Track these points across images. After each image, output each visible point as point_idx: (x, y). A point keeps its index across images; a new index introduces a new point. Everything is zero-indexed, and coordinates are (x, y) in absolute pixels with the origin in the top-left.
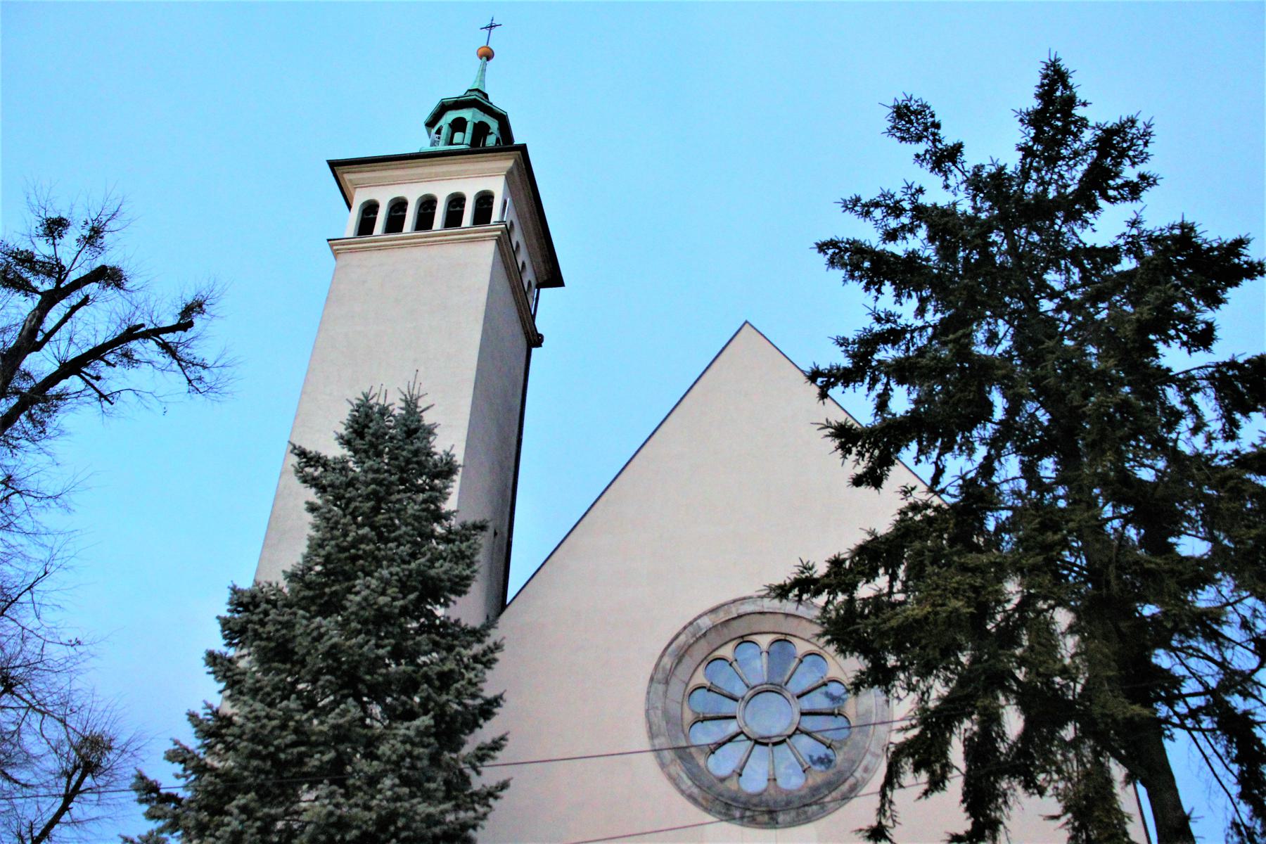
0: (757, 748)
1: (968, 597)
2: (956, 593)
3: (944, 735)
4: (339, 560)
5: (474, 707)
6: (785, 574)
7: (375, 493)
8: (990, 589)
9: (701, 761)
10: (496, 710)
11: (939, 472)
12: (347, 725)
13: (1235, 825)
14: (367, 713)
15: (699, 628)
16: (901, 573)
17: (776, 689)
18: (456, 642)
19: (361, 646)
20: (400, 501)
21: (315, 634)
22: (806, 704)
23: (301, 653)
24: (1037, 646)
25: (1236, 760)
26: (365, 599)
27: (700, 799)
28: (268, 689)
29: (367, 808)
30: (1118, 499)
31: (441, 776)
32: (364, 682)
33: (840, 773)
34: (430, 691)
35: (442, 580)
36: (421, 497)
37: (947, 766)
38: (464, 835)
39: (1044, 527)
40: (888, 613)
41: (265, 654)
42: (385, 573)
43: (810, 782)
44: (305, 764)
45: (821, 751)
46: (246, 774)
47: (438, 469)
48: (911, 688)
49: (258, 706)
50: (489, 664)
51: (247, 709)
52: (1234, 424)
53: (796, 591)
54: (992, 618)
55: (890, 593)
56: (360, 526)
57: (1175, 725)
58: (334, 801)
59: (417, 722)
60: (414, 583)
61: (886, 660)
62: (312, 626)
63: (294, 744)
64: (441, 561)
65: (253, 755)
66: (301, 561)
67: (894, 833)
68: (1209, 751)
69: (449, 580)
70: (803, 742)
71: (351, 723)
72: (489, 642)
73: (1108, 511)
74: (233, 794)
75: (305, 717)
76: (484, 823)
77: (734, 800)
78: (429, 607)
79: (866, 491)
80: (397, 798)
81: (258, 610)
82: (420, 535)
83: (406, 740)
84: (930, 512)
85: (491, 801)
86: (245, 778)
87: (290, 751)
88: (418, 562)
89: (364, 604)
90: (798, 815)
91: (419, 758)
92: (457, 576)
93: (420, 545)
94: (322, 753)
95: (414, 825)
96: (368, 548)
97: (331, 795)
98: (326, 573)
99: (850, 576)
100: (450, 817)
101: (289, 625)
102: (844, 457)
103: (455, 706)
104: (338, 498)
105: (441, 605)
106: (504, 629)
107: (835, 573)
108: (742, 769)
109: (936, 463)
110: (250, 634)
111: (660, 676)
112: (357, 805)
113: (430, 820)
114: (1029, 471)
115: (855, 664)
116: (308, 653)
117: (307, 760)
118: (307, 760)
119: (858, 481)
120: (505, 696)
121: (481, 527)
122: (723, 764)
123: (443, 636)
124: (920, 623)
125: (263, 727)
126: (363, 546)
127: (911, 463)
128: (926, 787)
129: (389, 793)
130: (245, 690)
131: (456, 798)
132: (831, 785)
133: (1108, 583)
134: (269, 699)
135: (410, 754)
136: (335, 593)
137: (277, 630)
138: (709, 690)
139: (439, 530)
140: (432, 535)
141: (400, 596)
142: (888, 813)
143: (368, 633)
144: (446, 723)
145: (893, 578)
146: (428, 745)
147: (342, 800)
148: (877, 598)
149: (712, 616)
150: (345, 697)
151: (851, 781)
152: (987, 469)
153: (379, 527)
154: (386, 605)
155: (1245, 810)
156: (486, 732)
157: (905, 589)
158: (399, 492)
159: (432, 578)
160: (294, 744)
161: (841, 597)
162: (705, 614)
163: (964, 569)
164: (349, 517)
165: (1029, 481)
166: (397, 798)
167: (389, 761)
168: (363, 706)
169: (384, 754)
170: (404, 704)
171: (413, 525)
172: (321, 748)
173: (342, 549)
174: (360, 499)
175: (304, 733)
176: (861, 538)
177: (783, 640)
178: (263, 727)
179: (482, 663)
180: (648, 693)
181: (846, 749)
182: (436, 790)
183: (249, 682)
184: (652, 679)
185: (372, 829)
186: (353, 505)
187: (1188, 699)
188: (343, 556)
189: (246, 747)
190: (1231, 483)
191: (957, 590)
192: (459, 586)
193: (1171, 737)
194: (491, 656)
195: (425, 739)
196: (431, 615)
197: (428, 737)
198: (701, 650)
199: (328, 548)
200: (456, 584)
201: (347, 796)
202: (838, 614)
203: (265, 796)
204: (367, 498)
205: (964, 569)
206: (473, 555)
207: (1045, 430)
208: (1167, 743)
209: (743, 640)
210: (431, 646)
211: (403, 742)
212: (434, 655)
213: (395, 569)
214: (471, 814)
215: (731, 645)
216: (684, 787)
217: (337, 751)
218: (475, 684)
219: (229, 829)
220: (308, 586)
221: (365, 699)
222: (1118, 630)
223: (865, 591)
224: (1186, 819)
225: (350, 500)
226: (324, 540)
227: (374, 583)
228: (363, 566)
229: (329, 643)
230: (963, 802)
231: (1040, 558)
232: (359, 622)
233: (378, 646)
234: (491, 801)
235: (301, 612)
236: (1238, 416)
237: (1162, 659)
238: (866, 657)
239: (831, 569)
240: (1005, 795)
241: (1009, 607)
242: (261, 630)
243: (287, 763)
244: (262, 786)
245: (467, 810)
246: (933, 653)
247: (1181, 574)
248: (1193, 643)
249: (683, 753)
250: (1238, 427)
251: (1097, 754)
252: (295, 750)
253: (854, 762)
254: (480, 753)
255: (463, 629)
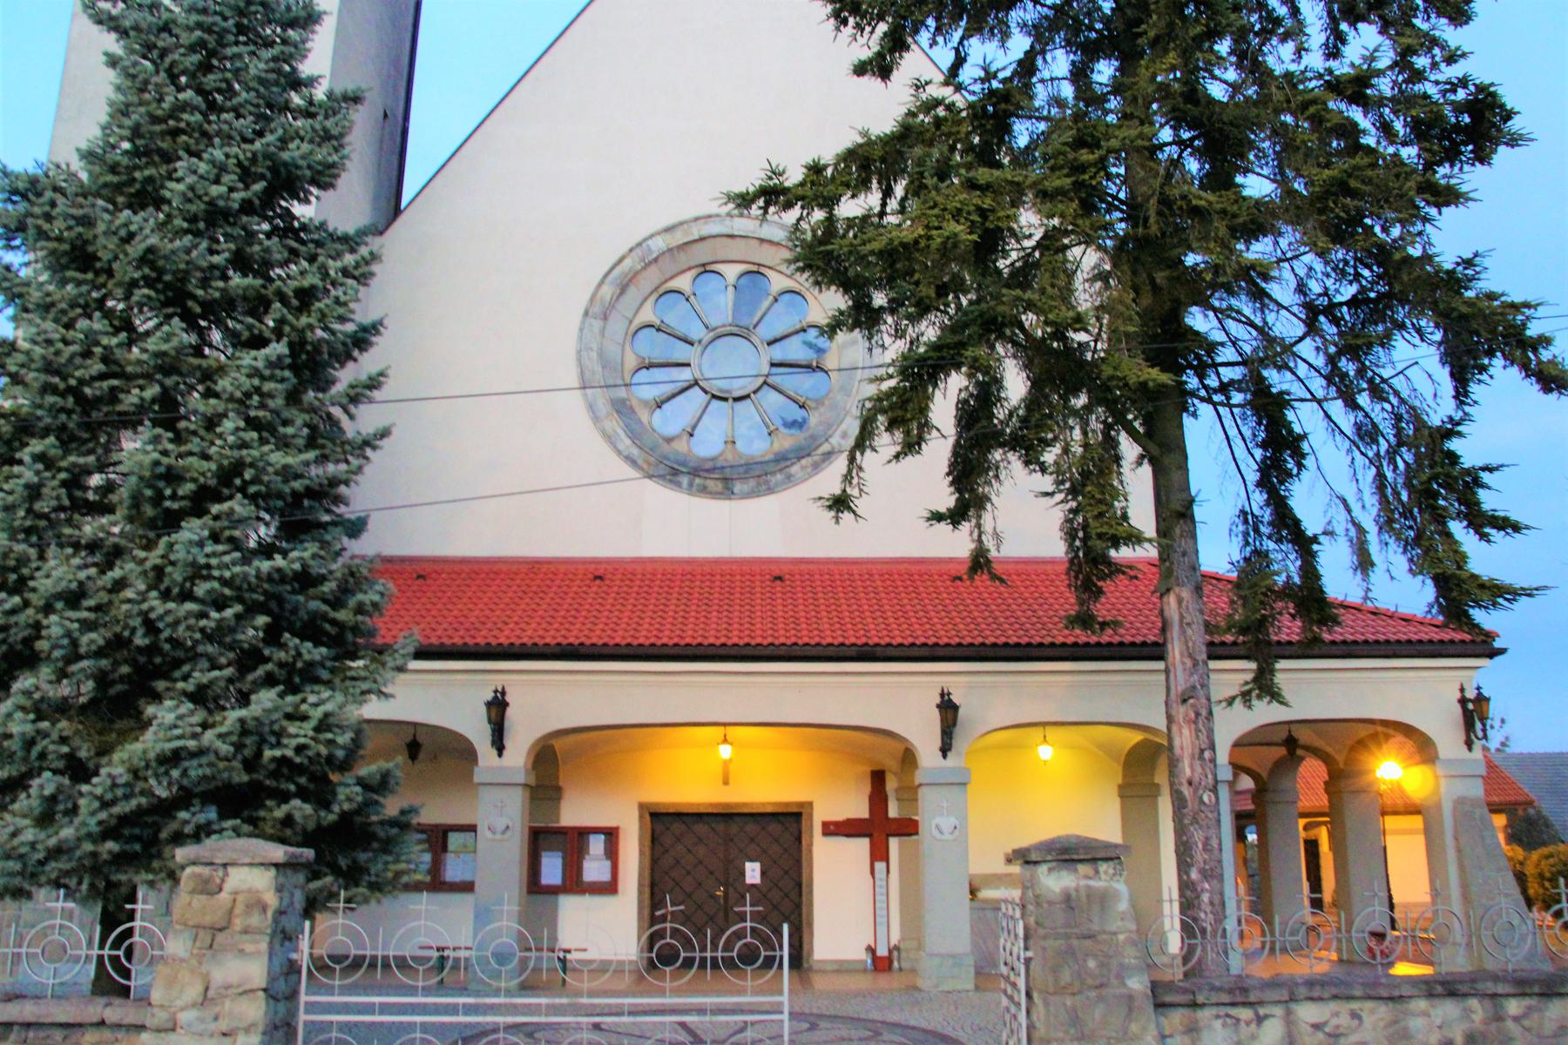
0: (716, 404)
1: (973, 222)
2: (957, 215)
3: (926, 390)
4: (152, 134)
5: (346, 335)
6: (751, 180)
7: (202, 44)
8: (1001, 214)
9: (644, 416)
10: (374, 339)
11: (960, 61)
12: (173, 353)
13: (1243, 513)
14: (205, 341)
15: (650, 249)
16: (899, 190)
17: (741, 332)
18: (319, 251)
19: (188, 251)
20: (239, 56)
21: (123, 233)
22: (778, 353)
23: (105, 258)
24: (1049, 289)
25: (1264, 445)
26: (192, 188)
27: (640, 462)
28: (64, 306)
29: (206, 457)
30: (1178, 119)
31: (300, 418)
32: (194, 297)
33: (813, 437)
34: (285, 311)
35: (298, 167)
36: (267, 54)
37: (925, 426)
38: (333, 491)
39: (1080, 143)
40: (871, 232)
41: (58, 260)
42: (218, 154)
43: (777, 447)
44: (119, 401)
45: (797, 414)
46: (39, 413)
47: (293, 14)
48: (899, 334)
49: (49, 325)
50: (363, 279)
51: (34, 330)
52: (1341, 38)
53: (761, 202)
54: (1005, 254)
55: (882, 214)
56: (180, 89)
57: (1202, 400)
58: (160, 447)
59: (264, 352)
60: (260, 170)
61: (871, 298)
62: (118, 222)
63: (102, 377)
64: (297, 141)
65: (47, 389)
66: (98, 132)
67: (860, 505)
68: (1233, 432)
69: (309, 167)
70: (771, 398)
71: (179, 350)
72: (364, 251)
73: (1166, 135)
74: (26, 439)
75: (114, 341)
76: (359, 478)
77: (683, 464)
78: (283, 203)
79: (871, 83)
80: (244, 445)
81: (42, 200)
82: (270, 106)
83: (255, 373)
84: (941, 112)
85: (369, 452)
86: (39, 419)
87: (97, 384)
88: (264, 141)
89: (190, 195)
90: (759, 484)
91: (270, 395)
92: (320, 163)
93: (268, 119)
94: (142, 388)
95: (266, 478)
96: (192, 119)
97: (156, 440)
98: (135, 153)
99: (831, 187)
100: (315, 471)
101: (87, 221)
102: (838, 29)
103: (320, 333)
104: (150, 46)
105: (299, 200)
106: (395, 244)
107: (813, 183)
108: (694, 427)
109: (957, 50)
110: (31, 231)
111: (597, 309)
112: (191, 454)
113: (287, 473)
114: (1080, 75)
115: (835, 300)
116: (116, 258)
117: (122, 396)
118: (122, 396)
119: (861, 69)
120: (386, 322)
121: (356, 99)
122: (669, 421)
123: (303, 243)
124: (910, 248)
125: (57, 353)
126: (185, 116)
127: (925, 44)
128: (898, 448)
129: (231, 439)
130: (31, 306)
131: (323, 447)
132: (801, 453)
133: (1146, 220)
134: (65, 319)
135: (258, 390)
136: (150, 180)
137: (70, 228)
138: (659, 330)
139: (296, 100)
140: (286, 107)
141: (241, 185)
142: (855, 481)
143: (197, 234)
144: (308, 353)
145: (887, 193)
146: (283, 380)
147: (170, 447)
148: (865, 219)
149: (668, 237)
150: (169, 317)
151: (825, 448)
152: (1027, 66)
153: (210, 93)
154: (220, 197)
155: (1259, 498)
156: (366, 364)
157: (902, 210)
158: (237, 43)
159: (285, 164)
160: (102, 377)
161: (819, 215)
162: (658, 233)
163: (971, 185)
164: (163, 74)
165: (1078, 89)
166: (244, 445)
167: (231, 399)
168: (201, 332)
169: (224, 391)
170: (250, 328)
171: (257, 91)
172: (141, 382)
173: (155, 120)
174: (182, 50)
175: (116, 362)
176: (851, 139)
177: (755, 273)
178: (57, 353)
179: (354, 278)
180: (581, 330)
181: (822, 409)
182: (294, 436)
183: (35, 295)
184: (586, 313)
185: (212, 482)
186: (168, 60)
187: (1221, 370)
188: (157, 128)
189: (36, 379)
190: (1312, 110)
191: (959, 211)
192: (324, 177)
193: (1194, 415)
194: (364, 269)
195: (278, 372)
196: (288, 215)
197: (282, 369)
198: (651, 278)
199: (135, 117)
200: (320, 173)
201: (178, 439)
202: (814, 235)
203: (67, 440)
204: (192, 49)
205: (971, 185)
206: (342, 135)
207: (1107, 21)
208: (1187, 420)
209: (705, 269)
210: (286, 254)
211: (249, 376)
212: (293, 267)
213: (235, 150)
214: (343, 467)
215: (690, 275)
216: (621, 447)
217: (162, 385)
218: (345, 304)
219: (22, 481)
220: (114, 168)
221: (203, 323)
222: (1152, 281)
223: (849, 208)
224: (1191, 502)
225: (164, 53)
226: (127, 105)
227: (203, 167)
228: (186, 143)
229: (143, 246)
230: (948, 474)
231: (1069, 181)
232: (185, 219)
233: (212, 252)
234: (369, 452)
235: (100, 202)
236: (1344, 26)
237: (1199, 320)
238: (846, 291)
239: (807, 176)
240: (997, 468)
241: (1028, 244)
242: (46, 226)
243: (97, 401)
244: (64, 427)
245: (337, 461)
246: (928, 291)
247: (1234, 216)
248: (1233, 302)
249: (622, 408)
250: (1344, 42)
251: (1108, 427)
252: (105, 384)
253: (830, 426)
254: (352, 393)
255: (331, 235)
